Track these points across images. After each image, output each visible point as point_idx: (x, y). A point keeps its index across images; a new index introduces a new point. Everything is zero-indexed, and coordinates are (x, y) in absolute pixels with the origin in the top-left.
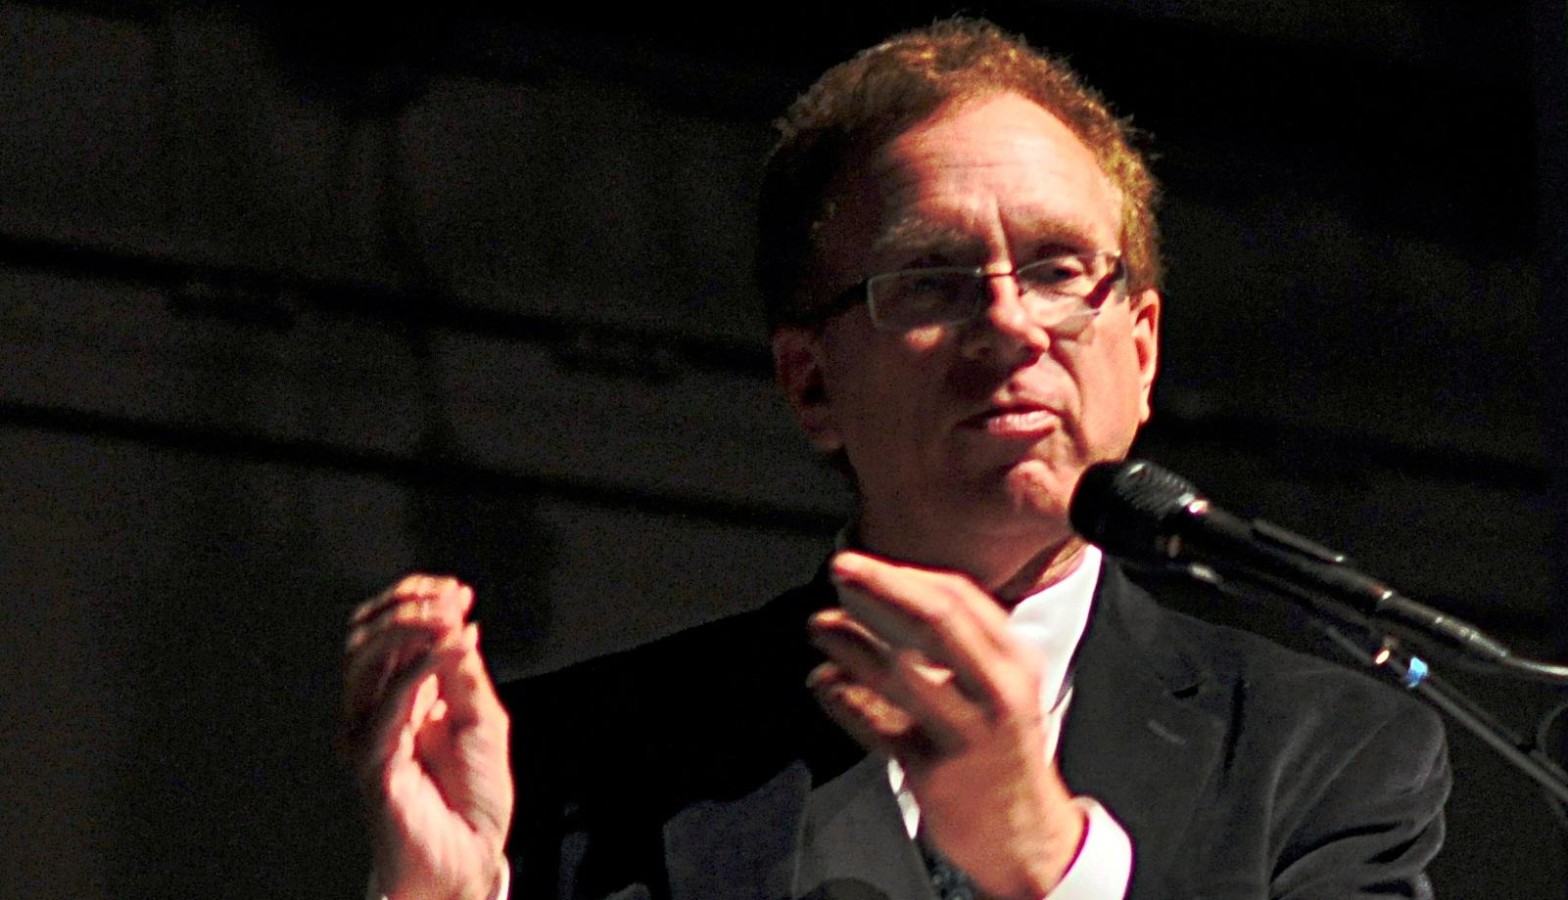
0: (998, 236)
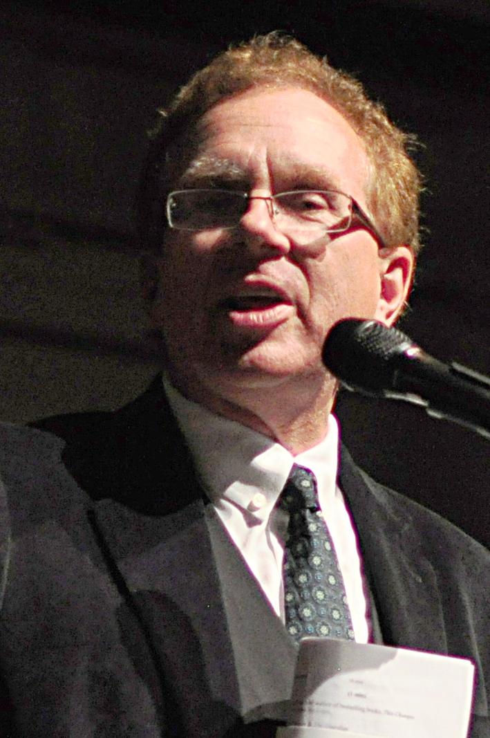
0: (264, 172)
